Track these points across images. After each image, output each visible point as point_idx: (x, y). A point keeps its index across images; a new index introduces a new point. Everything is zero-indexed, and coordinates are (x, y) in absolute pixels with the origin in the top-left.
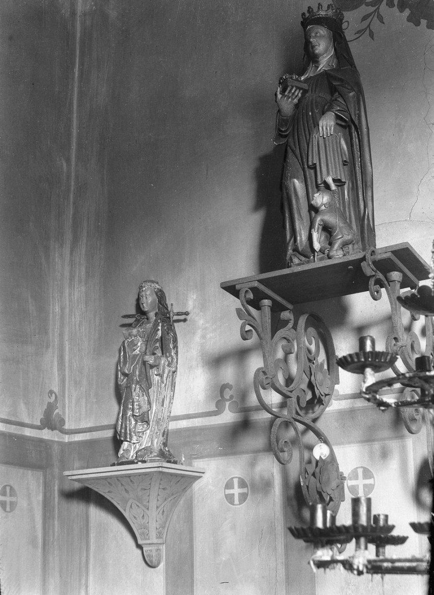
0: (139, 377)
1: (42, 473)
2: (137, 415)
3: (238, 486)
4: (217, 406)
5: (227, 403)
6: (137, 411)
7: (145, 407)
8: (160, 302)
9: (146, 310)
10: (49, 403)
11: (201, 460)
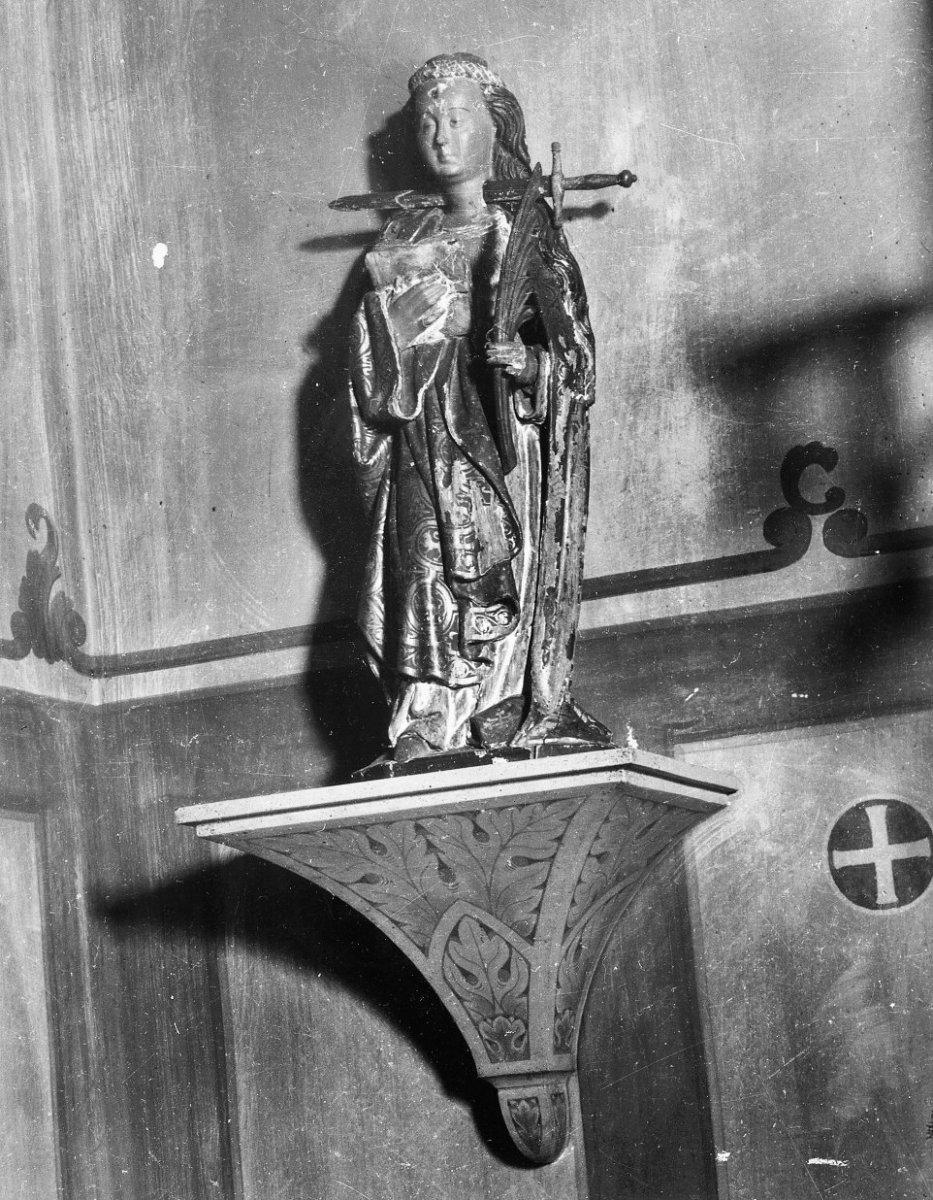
0: (458, 431)
1: (31, 825)
2: (470, 575)
3: (889, 834)
4: (769, 535)
5: (818, 523)
6: (469, 560)
7: (497, 546)
8: (503, 138)
9: (453, 169)
10: (33, 557)
11: (717, 743)
